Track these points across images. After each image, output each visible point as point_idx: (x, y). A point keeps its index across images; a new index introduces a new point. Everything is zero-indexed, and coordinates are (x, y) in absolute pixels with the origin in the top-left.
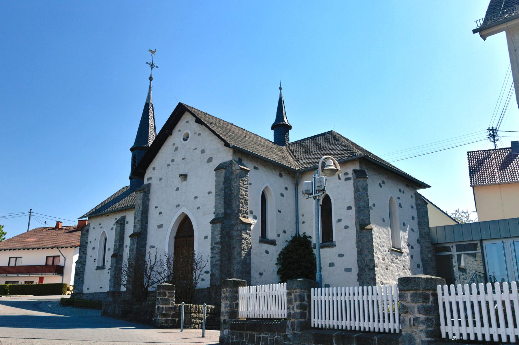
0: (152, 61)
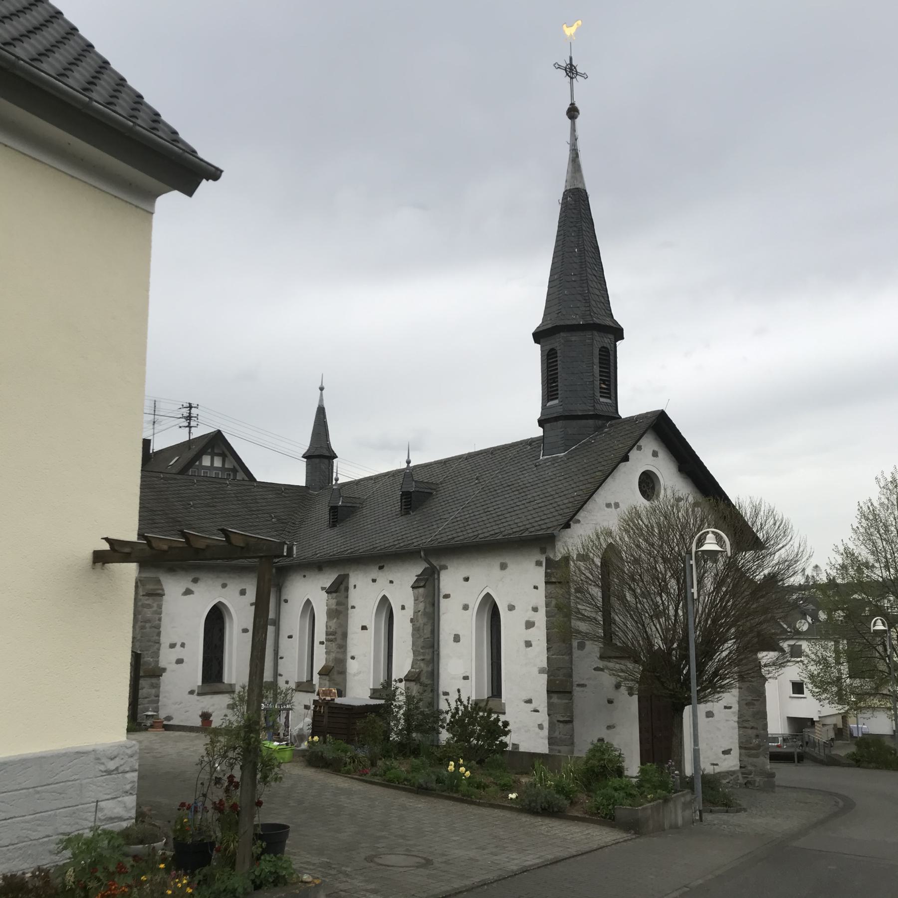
0: (571, 59)
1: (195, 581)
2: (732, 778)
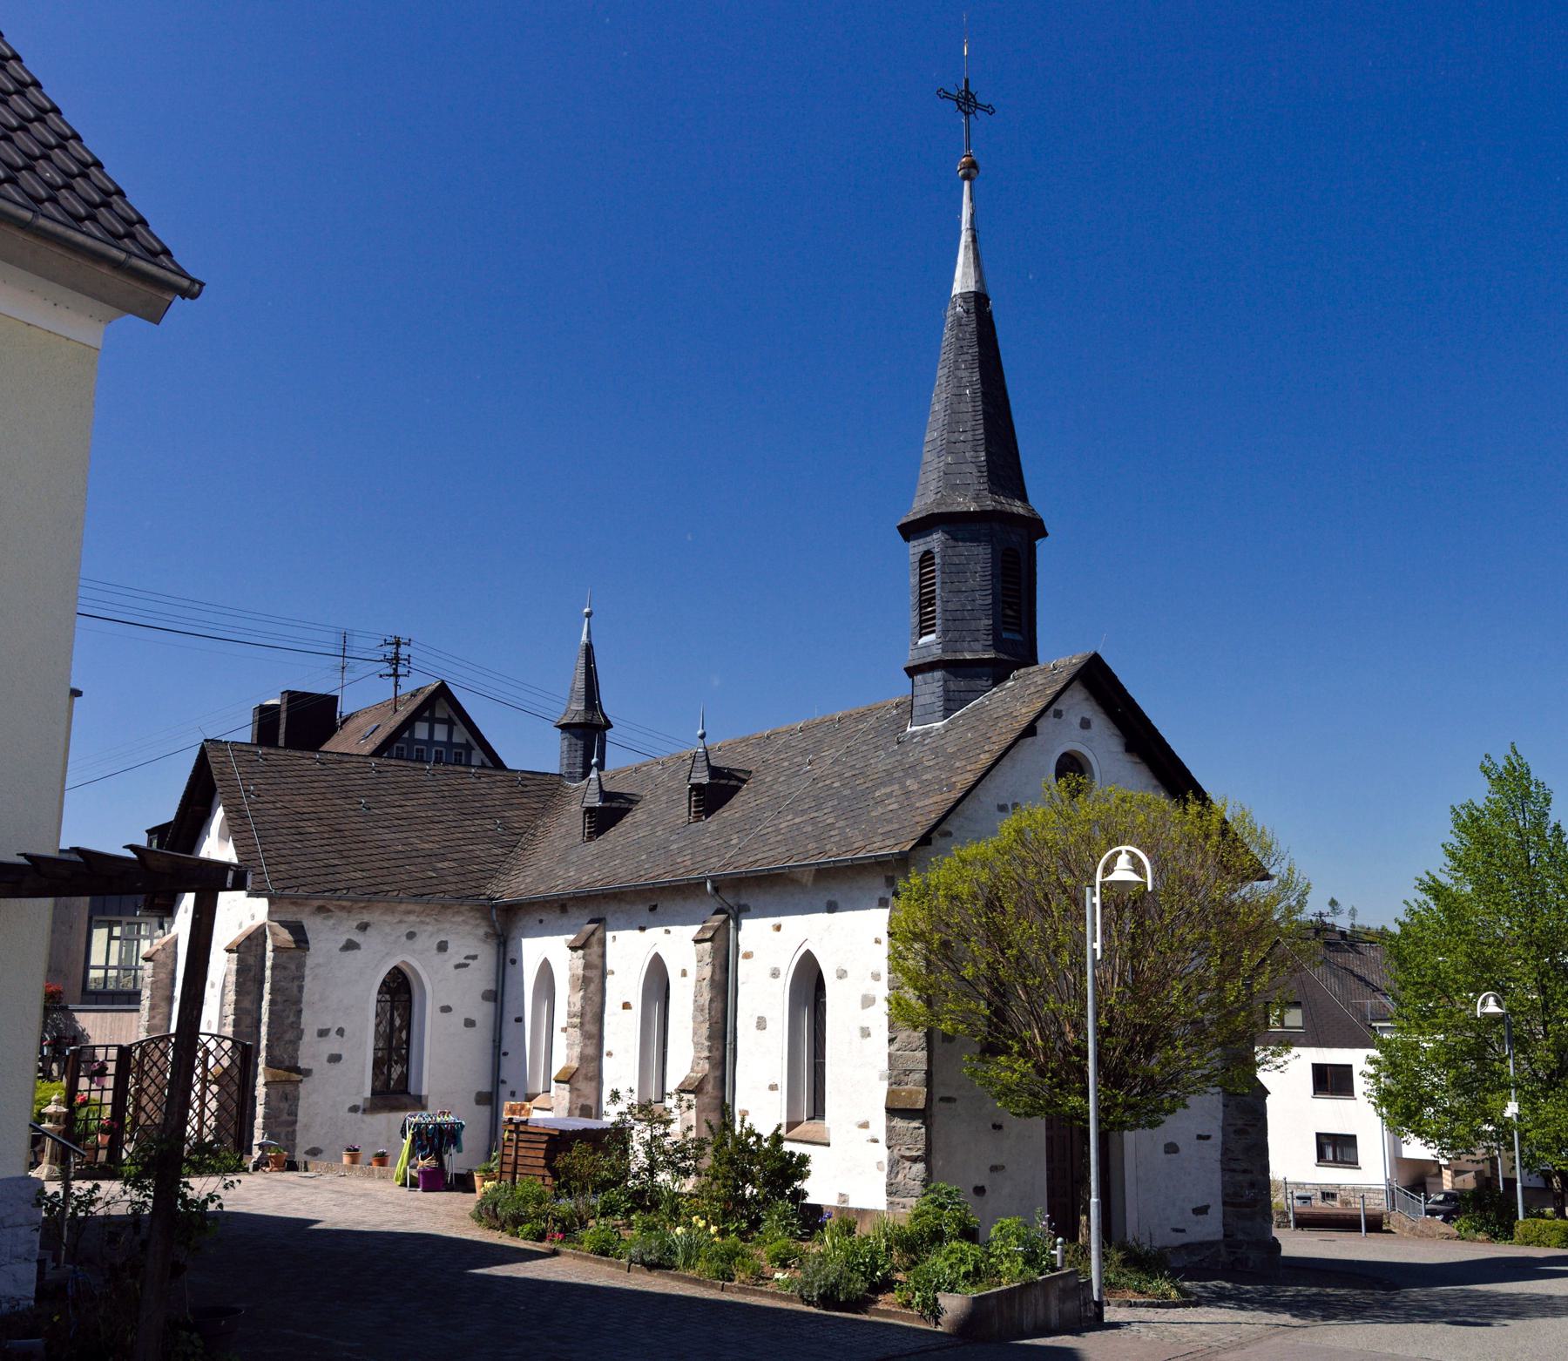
1: (363, 927)
2: (1208, 1253)
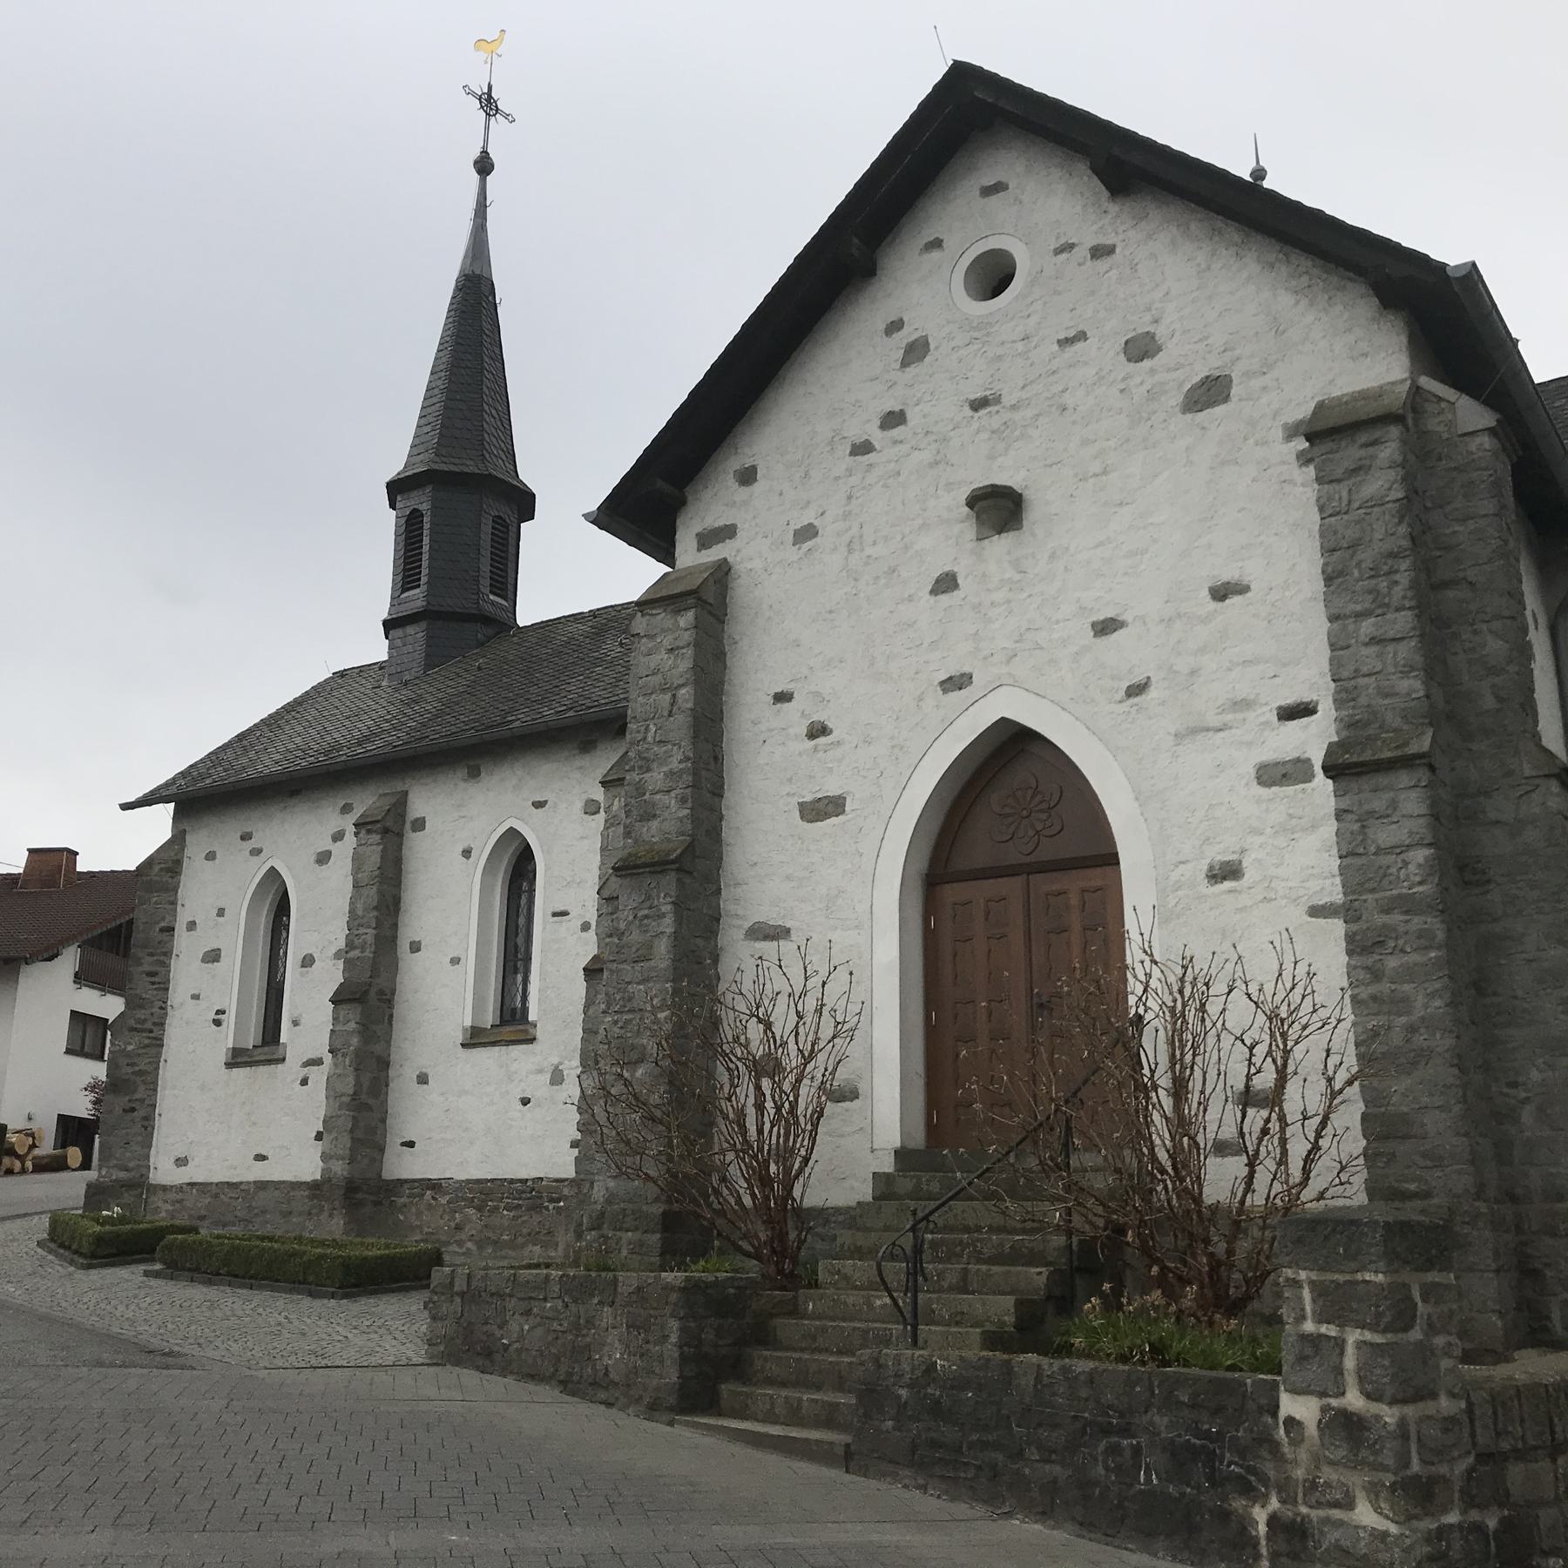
0: (490, 87)
